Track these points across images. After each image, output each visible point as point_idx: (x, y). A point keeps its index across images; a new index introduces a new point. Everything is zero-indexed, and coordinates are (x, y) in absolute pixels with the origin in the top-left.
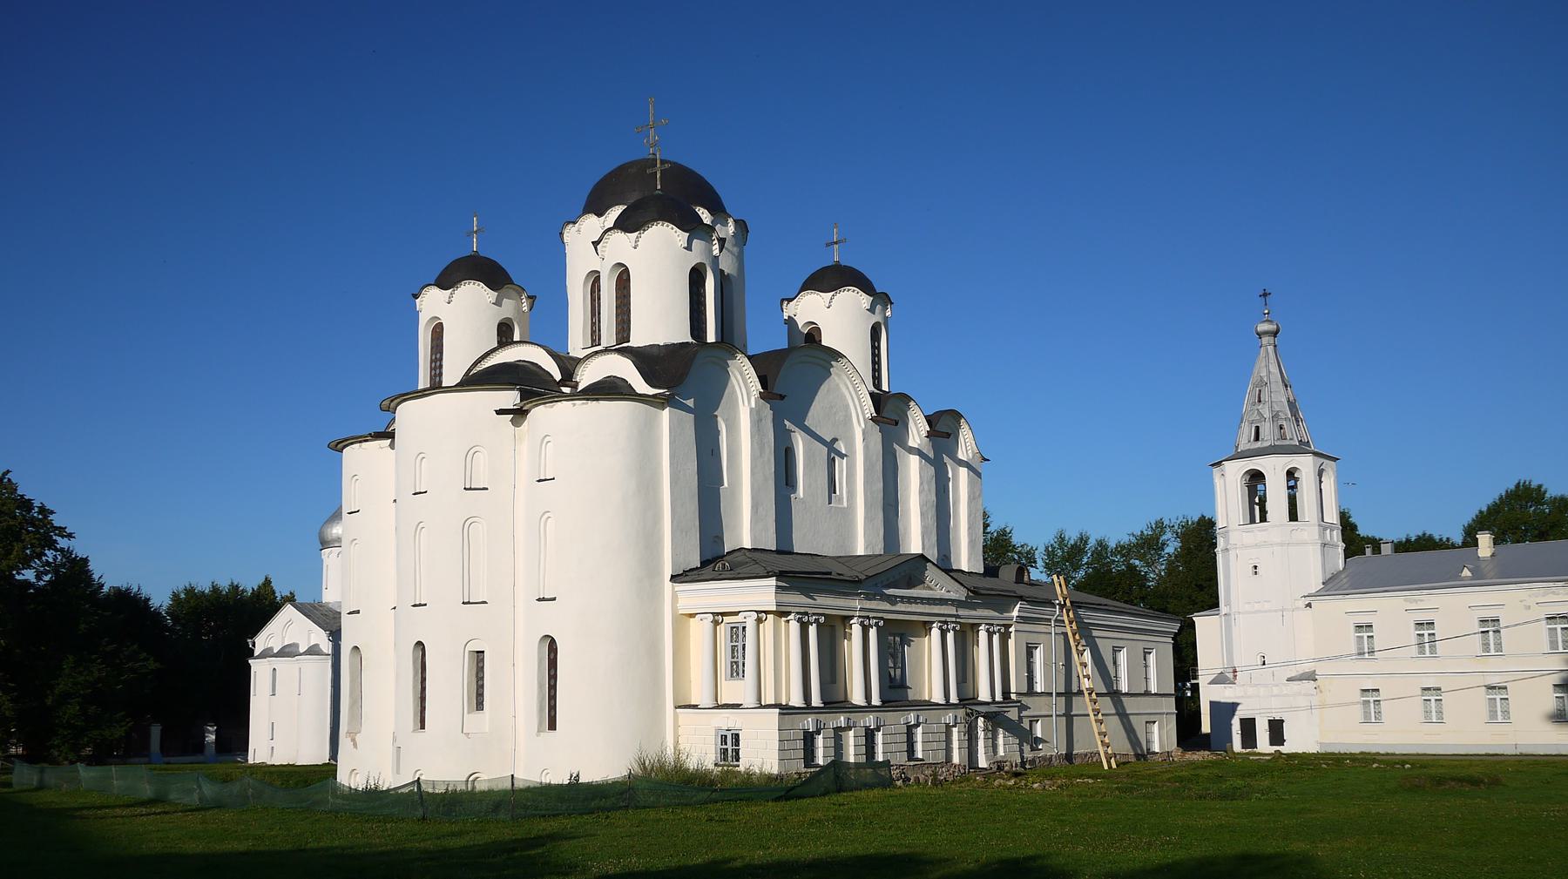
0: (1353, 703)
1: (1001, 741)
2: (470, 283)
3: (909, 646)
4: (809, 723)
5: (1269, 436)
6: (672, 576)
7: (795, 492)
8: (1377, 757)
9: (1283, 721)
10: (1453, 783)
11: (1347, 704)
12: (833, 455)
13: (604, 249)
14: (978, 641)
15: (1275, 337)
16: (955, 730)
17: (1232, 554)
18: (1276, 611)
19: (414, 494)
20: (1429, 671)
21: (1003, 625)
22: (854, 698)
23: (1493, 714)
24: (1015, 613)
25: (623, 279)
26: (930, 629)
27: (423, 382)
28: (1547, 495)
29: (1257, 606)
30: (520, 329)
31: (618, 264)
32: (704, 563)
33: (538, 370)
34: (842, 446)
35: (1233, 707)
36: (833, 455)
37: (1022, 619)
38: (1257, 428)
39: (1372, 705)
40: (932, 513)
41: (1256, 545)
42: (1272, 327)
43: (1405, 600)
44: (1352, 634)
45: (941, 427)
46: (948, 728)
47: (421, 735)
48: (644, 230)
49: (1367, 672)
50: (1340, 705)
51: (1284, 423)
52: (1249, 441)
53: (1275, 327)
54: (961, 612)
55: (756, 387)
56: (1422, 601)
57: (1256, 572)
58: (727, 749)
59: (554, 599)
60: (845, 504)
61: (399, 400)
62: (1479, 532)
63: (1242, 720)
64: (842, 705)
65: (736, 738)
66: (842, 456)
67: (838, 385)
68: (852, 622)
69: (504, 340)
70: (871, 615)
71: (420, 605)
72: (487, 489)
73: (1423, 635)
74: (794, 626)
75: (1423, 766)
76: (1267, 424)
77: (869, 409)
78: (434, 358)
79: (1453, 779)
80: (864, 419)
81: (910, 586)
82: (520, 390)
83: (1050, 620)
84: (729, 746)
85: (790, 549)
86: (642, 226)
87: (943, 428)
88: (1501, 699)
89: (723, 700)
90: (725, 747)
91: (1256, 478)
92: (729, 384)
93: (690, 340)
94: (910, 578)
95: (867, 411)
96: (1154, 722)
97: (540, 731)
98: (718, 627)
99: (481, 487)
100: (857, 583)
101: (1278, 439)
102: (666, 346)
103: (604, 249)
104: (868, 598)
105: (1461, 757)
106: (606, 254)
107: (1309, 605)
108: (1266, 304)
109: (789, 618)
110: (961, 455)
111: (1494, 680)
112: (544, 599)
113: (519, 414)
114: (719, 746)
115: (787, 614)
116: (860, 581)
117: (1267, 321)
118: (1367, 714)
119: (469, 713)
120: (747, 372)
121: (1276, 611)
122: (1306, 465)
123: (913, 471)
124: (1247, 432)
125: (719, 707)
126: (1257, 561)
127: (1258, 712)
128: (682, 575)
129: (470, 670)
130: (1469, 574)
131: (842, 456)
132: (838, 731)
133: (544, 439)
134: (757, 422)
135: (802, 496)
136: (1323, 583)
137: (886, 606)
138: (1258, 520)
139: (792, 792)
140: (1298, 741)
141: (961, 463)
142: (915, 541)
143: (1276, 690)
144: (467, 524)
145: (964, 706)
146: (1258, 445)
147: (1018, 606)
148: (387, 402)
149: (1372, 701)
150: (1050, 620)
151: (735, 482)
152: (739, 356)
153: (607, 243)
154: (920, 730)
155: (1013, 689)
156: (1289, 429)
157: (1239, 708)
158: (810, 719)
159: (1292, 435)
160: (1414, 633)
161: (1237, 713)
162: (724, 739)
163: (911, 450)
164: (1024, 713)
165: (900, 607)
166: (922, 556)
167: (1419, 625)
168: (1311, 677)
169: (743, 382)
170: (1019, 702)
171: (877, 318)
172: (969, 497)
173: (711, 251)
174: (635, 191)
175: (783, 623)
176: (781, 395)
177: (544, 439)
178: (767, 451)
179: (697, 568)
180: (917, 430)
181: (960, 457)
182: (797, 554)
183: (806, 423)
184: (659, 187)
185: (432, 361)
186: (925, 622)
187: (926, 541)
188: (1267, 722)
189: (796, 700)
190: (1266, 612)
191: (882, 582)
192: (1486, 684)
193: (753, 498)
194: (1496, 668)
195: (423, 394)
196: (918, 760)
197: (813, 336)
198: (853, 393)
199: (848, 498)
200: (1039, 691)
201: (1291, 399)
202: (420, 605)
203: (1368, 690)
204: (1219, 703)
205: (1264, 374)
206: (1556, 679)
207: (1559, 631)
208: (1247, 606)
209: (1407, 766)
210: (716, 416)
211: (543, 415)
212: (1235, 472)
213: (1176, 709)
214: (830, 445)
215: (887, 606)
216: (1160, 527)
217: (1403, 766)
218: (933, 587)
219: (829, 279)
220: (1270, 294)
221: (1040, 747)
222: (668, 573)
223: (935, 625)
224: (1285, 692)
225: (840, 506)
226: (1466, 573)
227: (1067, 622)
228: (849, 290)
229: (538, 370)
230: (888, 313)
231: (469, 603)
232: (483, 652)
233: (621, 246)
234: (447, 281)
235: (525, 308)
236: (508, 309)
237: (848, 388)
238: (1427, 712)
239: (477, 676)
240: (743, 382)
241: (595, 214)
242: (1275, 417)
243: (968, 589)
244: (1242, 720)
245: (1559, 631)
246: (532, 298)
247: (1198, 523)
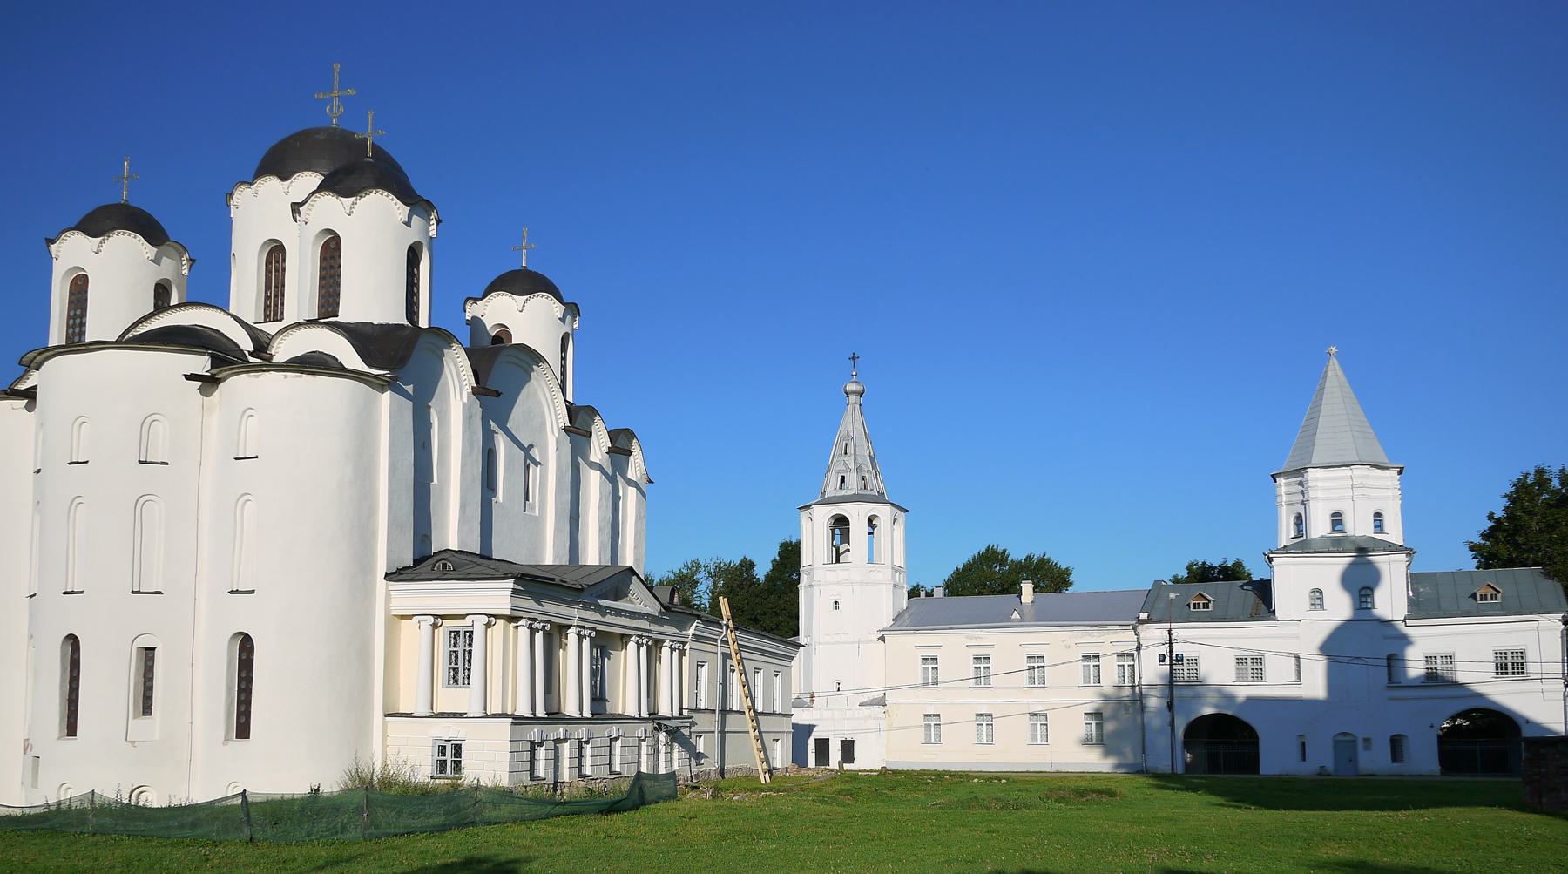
0: (917, 727)
1: (676, 755)
2: (124, 233)
3: (609, 659)
4: (535, 733)
5: (852, 486)
6: (387, 574)
7: (495, 497)
9: (853, 741)
10: (1094, 795)
11: (911, 727)
12: (528, 461)
13: (309, 212)
14: (660, 657)
16: (644, 744)
18: (853, 643)
19: (69, 464)
20: (983, 699)
21: (682, 643)
22: (567, 709)
23: (1034, 737)
24: (691, 631)
25: (331, 249)
26: (627, 643)
27: (56, 336)
28: (1010, 558)
30: (179, 293)
31: (270, 240)
32: (417, 562)
33: (221, 338)
34: (537, 453)
35: (810, 728)
36: (528, 461)
37: (697, 638)
39: (933, 728)
40: (608, 529)
42: (860, 388)
43: (967, 637)
44: (920, 665)
45: (621, 443)
46: (533, 747)
47: (71, 741)
48: (361, 197)
49: (929, 699)
54: (654, 628)
55: (470, 381)
58: (445, 761)
59: (252, 592)
60: (537, 513)
61: (51, 353)
62: (726, 599)
64: (555, 716)
65: (457, 749)
66: (537, 464)
67: (536, 390)
68: (569, 631)
69: (160, 303)
70: (587, 625)
71: (73, 593)
72: (167, 464)
74: (524, 632)
76: (852, 475)
77: (564, 420)
78: (72, 313)
79: (1094, 792)
80: (558, 426)
81: (617, 599)
82: (211, 356)
83: (716, 640)
84: (449, 757)
85: (490, 555)
86: (359, 192)
87: (621, 445)
89: (439, 709)
90: (443, 758)
91: (841, 522)
92: (443, 376)
93: (406, 323)
94: (617, 590)
95: (561, 420)
97: (227, 739)
98: (436, 631)
99: (159, 461)
100: (579, 591)
102: (381, 326)
103: (309, 212)
104: (586, 607)
105: (1036, 774)
106: (311, 219)
107: (882, 639)
109: (520, 623)
110: (630, 475)
111: (1037, 708)
112: (237, 592)
113: (209, 382)
114: (436, 757)
115: (519, 618)
116: (582, 590)
117: (855, 382)
118: (928, 736)
119: (134, 718)
120: (461, 364)
121: (853, 643)
122: (884, 512)
123: (593, 483)
124: (834, 480)
125: (488, 717)
126: (838, 597)
128: (395, 573)
129: (137, 669)
130: (1018, 617)
131: (537, 464)
132: (581, 745)
133: (247, 410)
134: (468, 418)
135: (501, 500)
136: (893, 620)
137: (597, 617)
138: (834, 561)
139: (616, 806)
140: (867, 760)
141: (630, 483)
142: (592, 554)
144: (141, 501)
145: (653, 720)
146: (843, 493)
147: (695, 624)
148: (31, 355)
149: (933, 725)
150: (716, 640)
151: (445, 479)
152: (455, 346)
153: (312, 205)
154: (619, 743)
155: (685, 705)
156: (871, 478)
157: (815, 729)
158: (536, 730)
160: (972, 665)
161: (813, 734)
162: (443, 750)
163: (592, 465)
164: (693, 729)
165: (609, 619)
166: (631, 569)
167: (977, 659)
168: (881, 702)
169: (457, 373)
170: (691, 718)
171: (567, 329)
172: (637, 516)
173: (428, 231)
174: (324, 159)
175: (512, 628)
176: (497, 392)
177: (247, 410)
178: (476, 450)
179: (410, 567)
180: (599, 446)
181: (629, 477)
182: (495, 559)
183: (508, 426)
184: (369, 154)
185: (69, 317)
186: (623, 636)
187: (602, 557)
189: (523, 710)
191: (597, 592)
193: (462, 498)
194: (1039, 698)
195: (59, 351)
196: (539, 779)
197: (502, 337)
198: (549, 401)
199: (540, 506)
200: (703, 708)
202: (73, 593)
203: (930, 715)
206: (1090, 708)
207: (1091, 666)
208: (826, 637)
210: (430, 407)
211: (238, 385)
214: (527, 450)
215: (597, 617)
216: (696, 566)
218: (634, 600)
219: (523, 282)
221: (702, 762)
222: (381, 570)
223: (633, 639)
224: (857, 716)
225: (533, 514)
226: (1016, 615)
227: (731, 643)
228: (543, 296)
229: (221, 338)
230: (576, 326)
231: (139, 592)
232: (154, 649)
233: (331, 211)
234: (96, 224)
235: (185, 271)
236: (168, 268)
237: (545, 395)
238: (980, 735)
239: (144, 677)
240: (457, 373)
241: (280, 178)
242: (859, 469)
243: (662, 605)
246: (192, 261)
247: (741, 564)
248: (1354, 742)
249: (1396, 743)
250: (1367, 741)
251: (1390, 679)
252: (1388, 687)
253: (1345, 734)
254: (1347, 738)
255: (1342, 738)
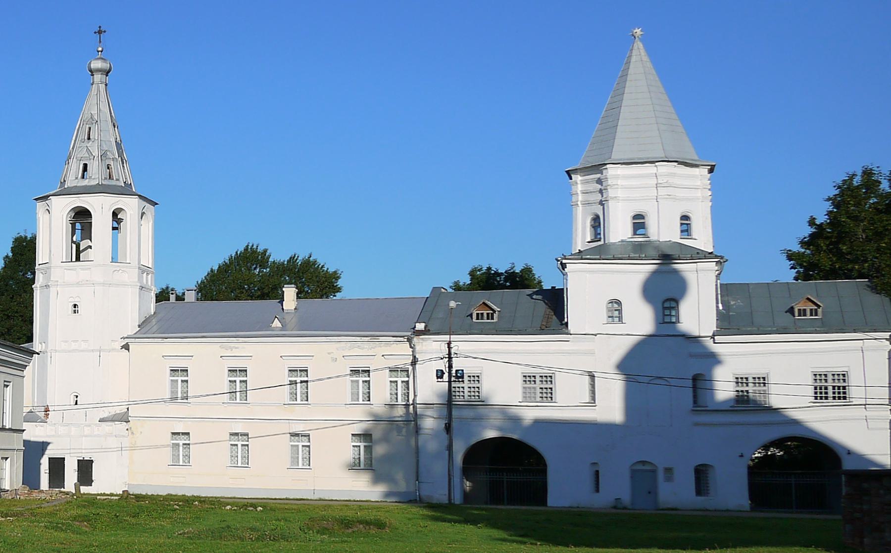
0: (164, 446)
5: (96, 175)
8: (221, 500)
9: (92, 461)
11: (157, 447)
15: (107, 76)
17: (53, 290)
23: (295, 460)
29: (74, 346)
38: (85, 166)
39: (181, 448)
41: (78, 283)
42: (106, 66)
50: (150, 447)
51: (112, 163)
52: (77, 178)
53: (109, 65)
56: (236, 348)
57: (75, 307)
62: (285, 286)
63: (51, 460)
73: (235, 381)
75: (361, 508)
76: (96, 163)
79: (361, 522)
88: (303, 446)
89: (587, 399)
91: (82, 216)
96: (6, 459)
101: (106, 178)
107: (126, 347)
108: (100, 42)
111: (298, 428)
118: (176, 457)
122: (130, 205)
124: (75, 168)
127: (69, 451)
130: (279, 325)
136: (139, 326)
143: (87, 431)
146: (85, 183)
149: (181, 444)
156: (116, 167)
157: (49, 447)
159: (119, 177)
161: (47, 452)
167: (232, 371)
168: (124, 418)
188: (48, 459)
190: (82, 351)
192: (291, 432)
201: (118, 139)
204: (30, 441)
205: (94, 112)
206: (358, 429)
209: (260, 508)
212: (62, 207)
213: (24, 446)
217: (256, 508)
220: (95, 33)
226: (277, 323)
238: (234, 457)
242: (103, 156)
244: (51, 460)
245: (361, 383)
248: (654, 472)
249: (701, 474)
250: (668, 470)
251: (695, 402)
252: (693, 410)
253: (644, 463)
254: (647, 467)
255: (640, 467)
